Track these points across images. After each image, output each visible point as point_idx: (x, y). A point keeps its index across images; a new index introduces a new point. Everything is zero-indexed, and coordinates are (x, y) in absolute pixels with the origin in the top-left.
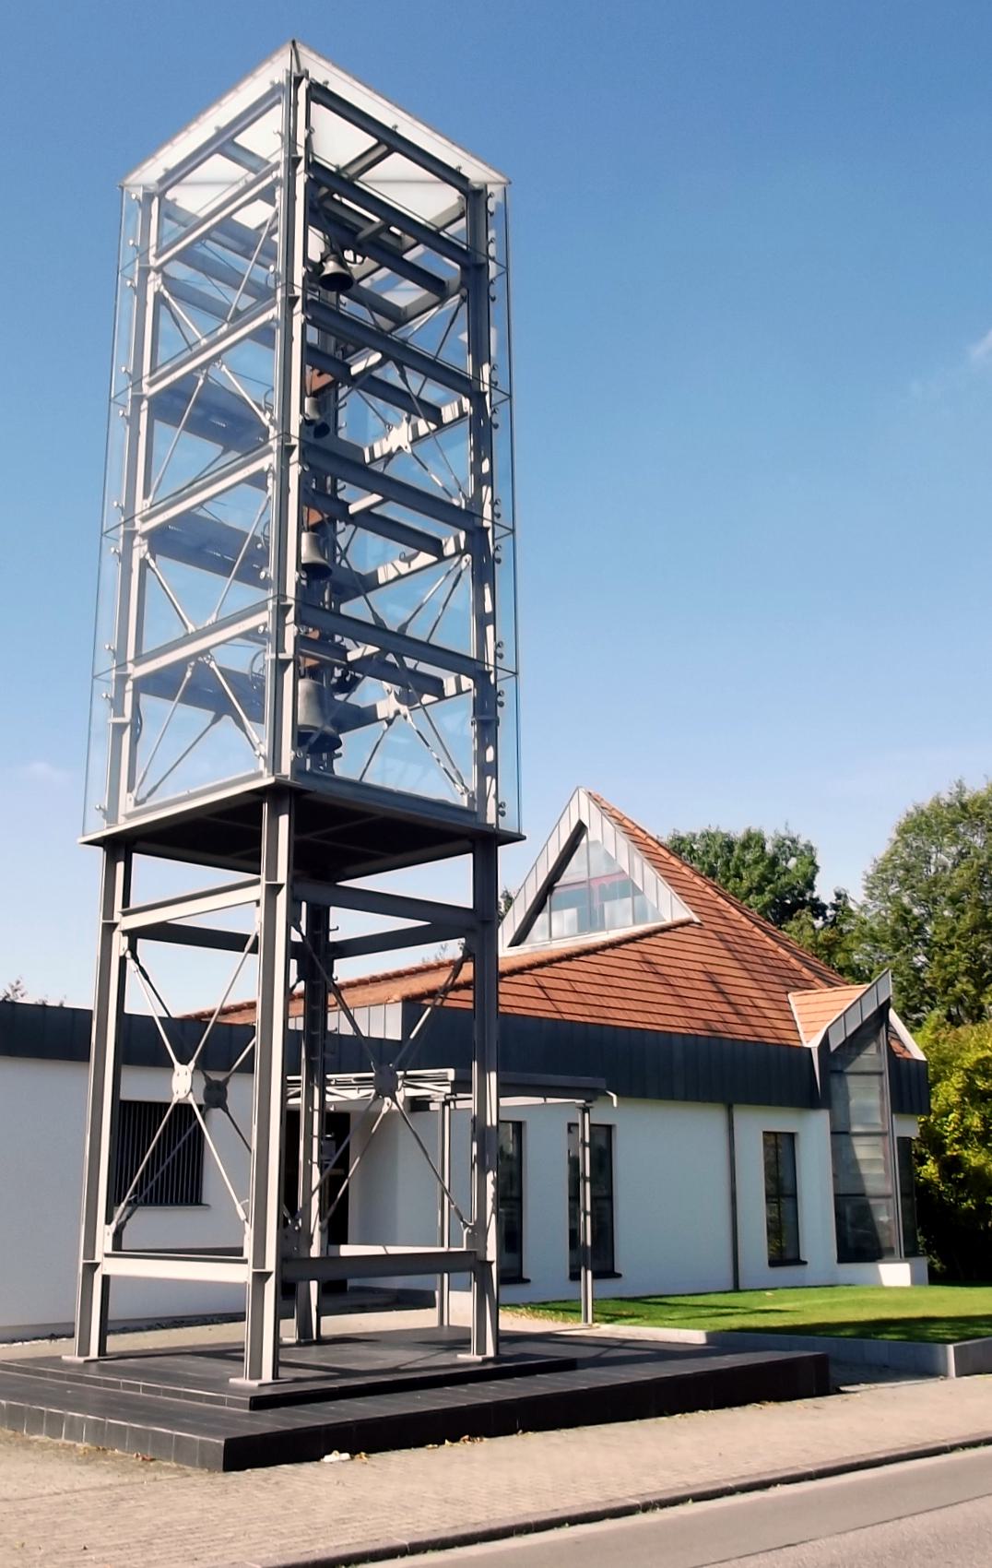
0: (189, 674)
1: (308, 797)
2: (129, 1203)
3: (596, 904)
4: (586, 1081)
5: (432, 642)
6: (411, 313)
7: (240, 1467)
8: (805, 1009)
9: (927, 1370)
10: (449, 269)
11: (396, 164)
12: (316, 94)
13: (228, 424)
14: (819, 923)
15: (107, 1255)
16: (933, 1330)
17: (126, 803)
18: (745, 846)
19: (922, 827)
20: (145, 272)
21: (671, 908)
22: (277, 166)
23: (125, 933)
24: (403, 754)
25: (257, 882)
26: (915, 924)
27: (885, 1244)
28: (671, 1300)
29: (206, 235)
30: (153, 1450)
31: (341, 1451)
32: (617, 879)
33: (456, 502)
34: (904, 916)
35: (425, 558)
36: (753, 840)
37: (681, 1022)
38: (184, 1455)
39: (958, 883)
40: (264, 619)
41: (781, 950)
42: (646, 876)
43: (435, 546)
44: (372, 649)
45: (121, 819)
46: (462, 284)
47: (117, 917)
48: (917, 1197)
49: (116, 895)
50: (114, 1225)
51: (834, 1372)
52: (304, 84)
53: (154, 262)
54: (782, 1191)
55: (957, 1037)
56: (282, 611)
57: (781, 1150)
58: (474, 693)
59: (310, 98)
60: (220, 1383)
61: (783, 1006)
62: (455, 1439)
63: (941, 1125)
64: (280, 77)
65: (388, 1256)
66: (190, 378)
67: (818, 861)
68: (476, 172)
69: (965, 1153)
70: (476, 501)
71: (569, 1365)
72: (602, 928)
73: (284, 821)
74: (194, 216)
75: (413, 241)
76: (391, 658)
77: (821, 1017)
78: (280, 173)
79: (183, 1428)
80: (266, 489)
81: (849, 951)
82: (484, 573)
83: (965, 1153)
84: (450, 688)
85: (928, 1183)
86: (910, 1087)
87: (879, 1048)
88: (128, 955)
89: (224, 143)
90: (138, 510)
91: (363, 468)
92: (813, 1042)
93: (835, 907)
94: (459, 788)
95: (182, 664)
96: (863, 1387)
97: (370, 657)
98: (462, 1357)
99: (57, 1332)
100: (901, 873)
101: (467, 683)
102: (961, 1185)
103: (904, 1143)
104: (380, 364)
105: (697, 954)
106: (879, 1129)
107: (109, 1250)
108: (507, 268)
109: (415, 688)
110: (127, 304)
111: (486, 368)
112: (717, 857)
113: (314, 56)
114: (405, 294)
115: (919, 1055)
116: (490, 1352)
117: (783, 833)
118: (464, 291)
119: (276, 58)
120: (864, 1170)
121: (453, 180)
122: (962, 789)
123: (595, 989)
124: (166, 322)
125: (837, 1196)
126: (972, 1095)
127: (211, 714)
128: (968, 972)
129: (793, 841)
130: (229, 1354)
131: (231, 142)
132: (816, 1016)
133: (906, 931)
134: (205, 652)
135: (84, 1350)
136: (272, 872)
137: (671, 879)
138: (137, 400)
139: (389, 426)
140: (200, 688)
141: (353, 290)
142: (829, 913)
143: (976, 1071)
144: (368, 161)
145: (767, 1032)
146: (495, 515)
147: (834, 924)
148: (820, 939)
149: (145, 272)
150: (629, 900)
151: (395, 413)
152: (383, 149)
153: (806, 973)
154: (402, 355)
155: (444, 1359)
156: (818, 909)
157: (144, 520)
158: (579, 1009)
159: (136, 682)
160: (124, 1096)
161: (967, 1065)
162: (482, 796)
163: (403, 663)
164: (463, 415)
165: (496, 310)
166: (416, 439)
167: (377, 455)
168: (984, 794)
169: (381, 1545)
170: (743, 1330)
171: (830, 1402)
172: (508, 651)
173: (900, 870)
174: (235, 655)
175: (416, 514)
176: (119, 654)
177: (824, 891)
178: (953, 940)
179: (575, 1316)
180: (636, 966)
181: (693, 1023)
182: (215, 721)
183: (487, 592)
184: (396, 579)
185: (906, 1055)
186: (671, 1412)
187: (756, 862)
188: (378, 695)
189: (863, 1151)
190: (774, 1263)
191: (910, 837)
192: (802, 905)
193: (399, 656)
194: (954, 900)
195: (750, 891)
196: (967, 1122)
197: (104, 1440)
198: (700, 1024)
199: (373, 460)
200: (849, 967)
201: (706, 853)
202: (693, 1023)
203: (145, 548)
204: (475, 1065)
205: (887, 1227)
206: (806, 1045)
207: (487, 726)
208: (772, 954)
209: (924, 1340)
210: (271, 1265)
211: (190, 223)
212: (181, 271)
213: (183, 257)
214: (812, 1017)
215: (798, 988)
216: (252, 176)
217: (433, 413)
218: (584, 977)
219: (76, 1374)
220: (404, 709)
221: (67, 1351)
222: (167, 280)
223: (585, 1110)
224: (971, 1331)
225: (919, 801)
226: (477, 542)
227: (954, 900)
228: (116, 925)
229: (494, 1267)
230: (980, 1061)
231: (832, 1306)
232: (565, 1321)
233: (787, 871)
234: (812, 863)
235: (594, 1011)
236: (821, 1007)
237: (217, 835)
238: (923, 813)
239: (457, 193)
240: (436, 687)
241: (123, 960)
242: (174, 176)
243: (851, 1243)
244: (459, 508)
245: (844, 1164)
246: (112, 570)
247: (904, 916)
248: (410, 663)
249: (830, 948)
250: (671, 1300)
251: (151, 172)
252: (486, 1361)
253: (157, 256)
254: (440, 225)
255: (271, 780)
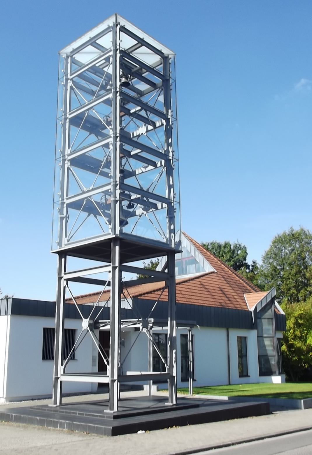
0: (84, 203)
1: (124, 240)
2: (68, 359)
3: (184, 266)
4: (191, 322)
5: (153, 193)
6: (145, 93)
7: (116, 435)
8: (249, 299)
9: (296, 407)
10: (158, 80)
11: (144, 49)
12: (121, 29)
13: (94, 127)
14: (248, 271)
15: (62, 375)
16: (295, 396)
17: (65, 241)
18: (225, 247)
19: (280, 241)
20: (67, 80)
21: (207, 268)
22: (111, 51)
23: (65, 280)
24: (147, 226)
25: (110, 265)
26: (278, 272)
27: (273, 370)
28: (212, 388)
29: (87, 70)
30: (90, 431)
31: (142, 430)
32: (191, 258)
33: (161, 151)
34: (275, 269)
35: (151, 167)
36: (227, 245)
37: (213, 303)
38: (99, 432)
39: (291, 258)
40: (110, 187)
41: (241, 281)
42: (200, 258)
43: (154, 164)
44: (139, 196)
45: (63, 246)
46: (162, 85)
47: (63, 275)
48: (282, 355)
49: (61, 268)
50: (64, 366)
51: (271, 409)
52: (119, 26)
53: (69, 77)
54: (243, 355)
55: (292, 307)
56: (116, 185)
57: (242, 342)
58: (167, 209)
59: (120, 30)
60: (102, 412)
61: (243, 298)
62: (171, 427)
63: (288, 334)
64: (111, 25)
65: (142, 375)
66: (83, 113)
67: (248, 252)
68: (166, 51)
69: (295, 342)
70: (167, 151)
71: (197, 406)
72: (186, 274)
73: (117, 248)
74: (84, 64)
75: (145, 71)
76: (145, 199)
77: (254, 301)
78: (111, 53)
79: (97, 424)
80: (109, 148)
81: (257, 280)
82: (170, 172)
83: (295, 342)
84: (159, 206)
85: (284, 351)
86: (280, 322)
87: (272, 311)
88: (66, 286)
89: (93, 42)
90: (66, 153)
91: (130, 139)
92: (252, 309)
93: (253, 266)
94: (163, 236)
95: (82, 200)
96: (278, 412)
97: (139, 198)
98: (166, 404)
99: (34, 398)
100: (273, 256)
101: (165, 205)
102: (293, 352)
103: (279, 339)
104: (140, 110)
105: (216, 282)
106: (272, 336)
107: (62, 373)
108: (175, 81)
109: (148, 206)
110: (61, 90)
111: (170, 111)
112: (216, 250)
113: (121, 18)
114: (143, 87)
115: (283, 313)
116: (175, 402)
117: (237, 243)
118: (163, 88)
119: (110, 18)
120: (267, 348)
121: (160, 54)
122: (292, 230)
123: (188, 293)
124: (73, 95)
125: (259, 356)
126: (297, 325)
127: (87, 214)
128: (294, 287)
129: (240, 245)
130: (104, 404)
131: (95, 42)
132: (253, 301)
133: (275, 274)
134: (90, 196)
135: (55, 403)
136: (114, 263)
137: (208, 258)
138: (66, 119)
139: (139, 127)
140: (89, 208)
141: (129, 87)
142: (251, 268)
143: (298, 317)
144: (135, 48)
145: (238, 306)
146: (173, 155)
147: (252, 271)
148: (249, 276)
149: (67, 80)
150: (194, 265)
151: (139, 122)
152: (140, 45)
153: (249, 288)
154: (145, 107)
155: (160, 405)
156: (247, 266)
157: (69, 155)
158: (183, 299)
159: (67, 204)
160: (65, 328)
161: (296, 316)
162: (170, 239)
163: (148, 200)
164: (162, 125)
165: (172, 93)
166: (147, 131)
167: (135, 135)
168: (299, 231)
169: (305, 428)
170: (239, 396)
171: (271, 416)
172: (177, 196)
173: (273, 255)
174: (96, 196)
175: (148, 154)
176: (62, 196)
177: (249, 261)
178: (290, 277)
179: (187, 393)
180: (199, 286)
181: (216, 303)
182: (89, 215)
183: (171, 178)
184: (141, 173)
185: (279, 313)
186: (228, 419)
187: (228, 252)
188: (139, 210)
189: (267, 342)
190: (240, 376)
191: (276, 244)
192: (242, 265)
193: (147, 198)
194: (290, 264)
195: (226, 261)
196: (296, 333)
197: (72, 429)
198: (218, 304)
199: (134, 137)
200: (257, 285)
201: (213, 249)
202: (216, 303)
203: (69, 164)
204: (169, 319)
205: (274, 365)
206: (250, 310)
207: (171, 218)
208: (238, 282)
209: (293, 398)
210: (116, 377)
211: (82, 66)
212: (77, 80)
213: (79, 76)
214: (251, 302)
215: (246, 292)
216: (102, 54)
217: (153, 124)
218: (184, 289)
219: (55, 410)
220: (145, 213)
221: (50, 403)
222: (74, 82)
223: (190, 331)
224: (306, 396)
225: (279, 233)
226: (168, 163)
227: (290, 264)
228: (62, 277)
229: (175, 378)
230: (300, 314)
231: (261, 389)
232: (184, 394)
233: (238, 255)
234: (246, 252)
235: (188, 300)
236: (254, 298)
237: (97, 251)
238: (280, 237)
239: (160, 57)
240: (155, 206)
241: (65, 288)
242: (76, 51)
243: (263, 370)
244: (161, 153)
245: (261, 346)
246: (59, 171)
247: (275, 269)
248: (148, 199)
249: (252, 279)
250: (212, 388)
251: (69, 49)
252: (174, 405)
253: (71, 75)
254: (154, 66)
255: (114, 236)
